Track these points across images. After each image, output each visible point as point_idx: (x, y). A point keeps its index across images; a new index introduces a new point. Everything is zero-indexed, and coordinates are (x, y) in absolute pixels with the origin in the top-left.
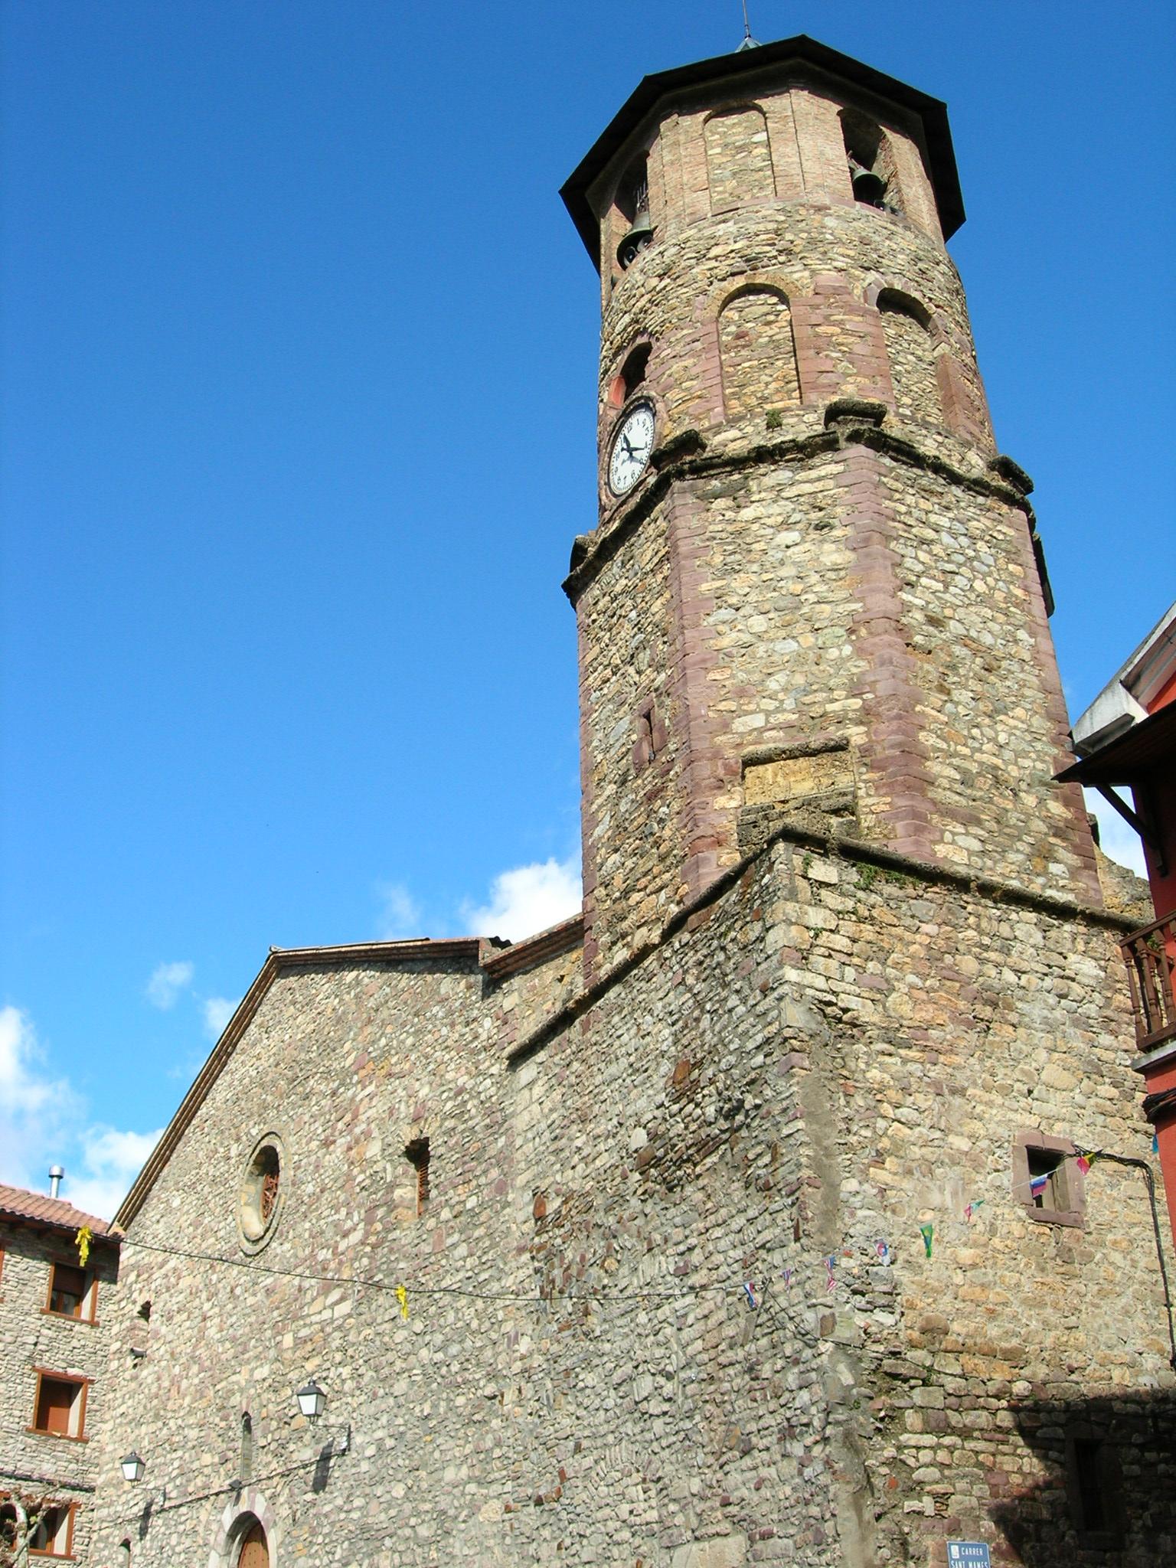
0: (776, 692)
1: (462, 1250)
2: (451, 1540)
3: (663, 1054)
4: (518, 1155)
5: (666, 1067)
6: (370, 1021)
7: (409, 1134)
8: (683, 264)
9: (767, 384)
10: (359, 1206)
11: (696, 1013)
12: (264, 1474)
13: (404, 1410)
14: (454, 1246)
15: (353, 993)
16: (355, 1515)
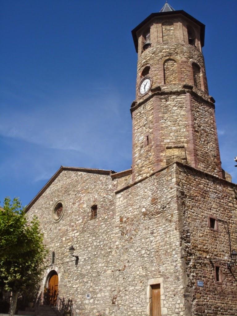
0: (172, 136)
1: (104, 226)
2: (100, 277)
3: (149, 196)
4: (117, 210)
5: (150, 198)
6: (84, 182)
7: (92, 204)
8: (157, 52)
9: (172, 78)
10: (82, 216)
11: (157, 190)
12: (57, 263)
13: (90, 253)
14: (102, 225)
15: (80, 177)
16: (79, 271)
